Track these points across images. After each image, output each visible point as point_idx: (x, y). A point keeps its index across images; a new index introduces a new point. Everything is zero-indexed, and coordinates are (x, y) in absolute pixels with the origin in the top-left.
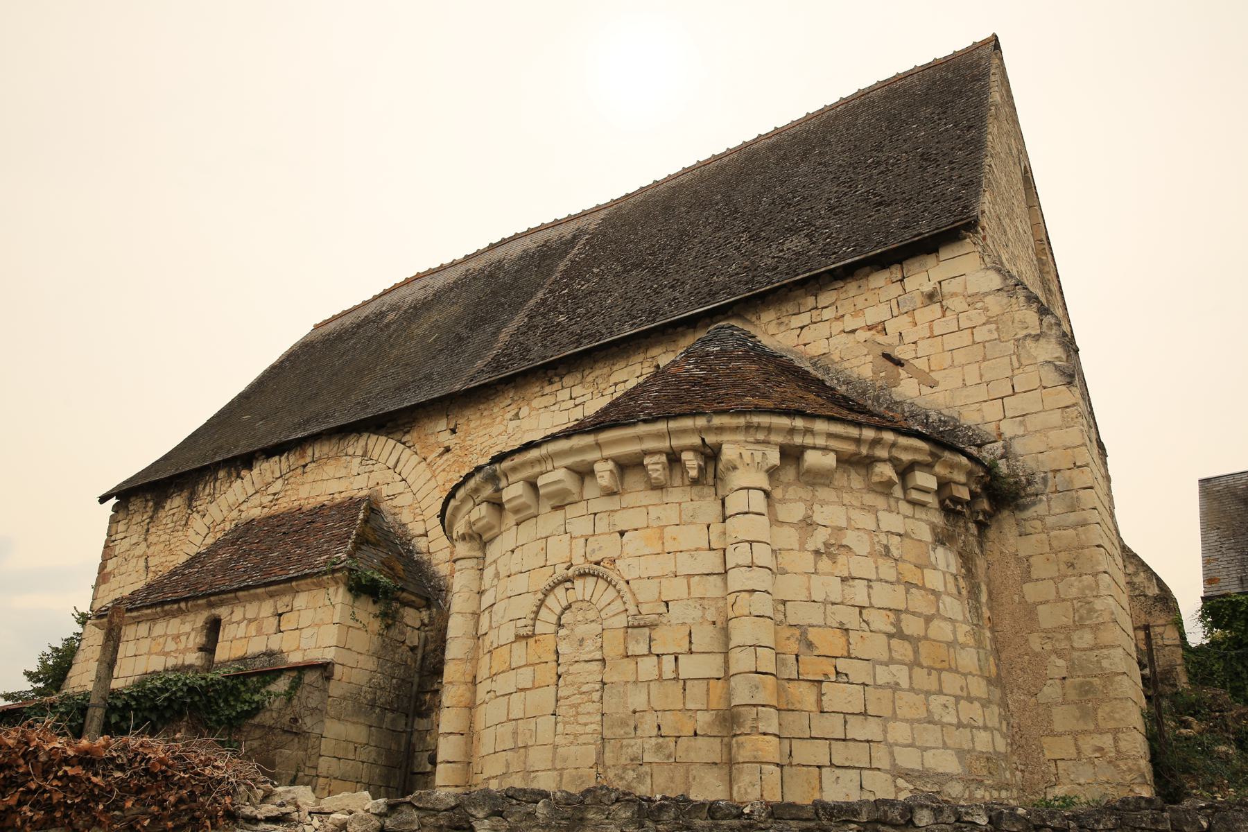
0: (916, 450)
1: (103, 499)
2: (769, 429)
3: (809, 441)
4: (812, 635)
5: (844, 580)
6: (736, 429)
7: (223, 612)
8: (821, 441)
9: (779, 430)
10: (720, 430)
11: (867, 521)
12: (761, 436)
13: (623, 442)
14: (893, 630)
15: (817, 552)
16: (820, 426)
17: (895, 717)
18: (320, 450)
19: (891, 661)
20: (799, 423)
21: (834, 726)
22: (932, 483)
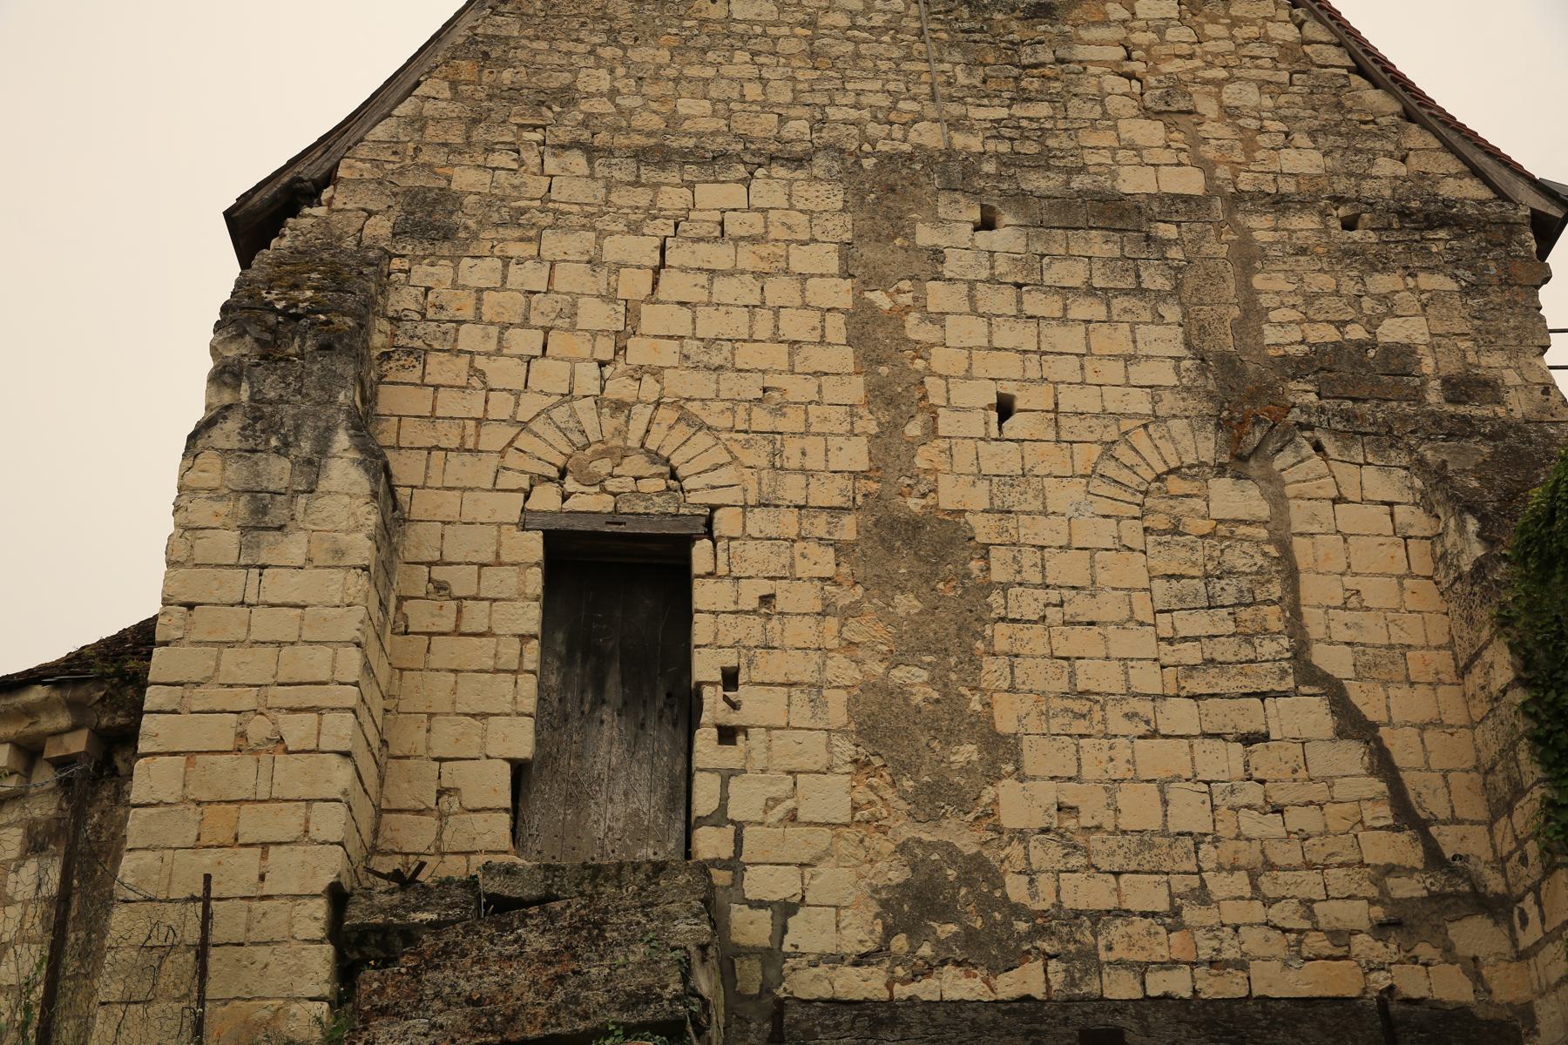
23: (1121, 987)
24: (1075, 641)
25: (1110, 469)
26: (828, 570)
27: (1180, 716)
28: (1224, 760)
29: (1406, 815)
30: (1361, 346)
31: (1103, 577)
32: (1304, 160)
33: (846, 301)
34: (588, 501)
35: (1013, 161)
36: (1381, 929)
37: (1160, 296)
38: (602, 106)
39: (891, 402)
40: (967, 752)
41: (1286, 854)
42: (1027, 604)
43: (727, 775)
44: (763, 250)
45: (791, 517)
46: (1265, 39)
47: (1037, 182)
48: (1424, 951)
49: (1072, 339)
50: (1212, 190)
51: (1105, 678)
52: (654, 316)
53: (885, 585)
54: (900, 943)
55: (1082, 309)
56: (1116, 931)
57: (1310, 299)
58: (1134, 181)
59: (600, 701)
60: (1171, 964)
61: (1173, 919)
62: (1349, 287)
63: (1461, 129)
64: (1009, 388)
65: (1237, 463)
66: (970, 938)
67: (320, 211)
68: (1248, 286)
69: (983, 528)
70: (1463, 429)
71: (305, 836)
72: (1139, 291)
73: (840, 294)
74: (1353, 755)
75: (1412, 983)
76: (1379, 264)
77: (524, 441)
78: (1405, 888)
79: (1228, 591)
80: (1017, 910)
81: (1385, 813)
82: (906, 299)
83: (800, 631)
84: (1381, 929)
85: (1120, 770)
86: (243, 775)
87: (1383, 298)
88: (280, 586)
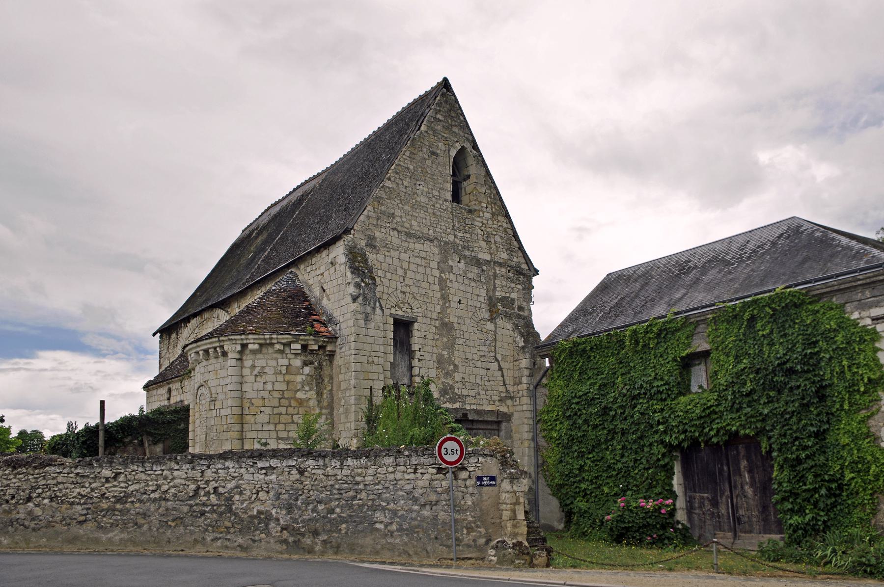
0: (287, 338)
1: (154, 335)
2: (236, 340)
3: (248, 341)
4: (253, 401)
5: (264, 383)
6: (227, 340)
7: (171, 386)
8: (252, 341)
9: (238, 340)
10: (223, 341)
11: (274, 363)
12: (234, 342)
13: (204, 345)
14: (281, 397)
15: (256, 375)
16: (250, 337)
17: (279, 423)
18: (206, 315)
19: (280, 406)
20: (243, 337)
21: (259, 427)
22: (299, 347)
23: (468, 407)
24: (467, 349)
25: (474, 317)
26: (434, 332)
27: (479, 364)
28: (484, 372)
29: (504, 384)
30: (509, 297)
31: (375, 220)
32: (504, 255)
33: (438, 275)
34: (400, 313)
35: (463, 247)
36: (499, 401)
37: (484, 283)
38: (399, 220)
39: (444, 299)
40: (451, 367)
41: (489, 388)
42: (461, 341)
43: (420, 368)
44: (426, 261)
45: (429, 320)
46: (502, 226)
47: (467, 253)
48: (504, 404)
49: (470, 289)
50: (492, 260)
51: (469, 356)
52: (410, 274)
53: (441, 335)
54: (442, 398)
55: (473, 284)
56: (468, 398)
57: (503, 286)
58: (481, 256)
59: (397, 349)
60: (474, 404)
61: (475, 397)
62: (508, 285)
63: (530, 260)
64: (461, 298)
65: (492, 319)
66: (450, 398)
67: (351, 236)
68: (494, 282)
69: (456, 327)
70: (519, 317)
71: (378, 379)
72: (480, 281)
73: (436, 273)
74: (500, 373)
75: (501, 409)
76: (512, 281)
77: (390, 298)
78: (503, 395)
79: (488, 343)
80: (456, 394)
81: (502, 383)
82: (447, 277)
83: (430, 342)
84: (499, 401)
85: (471, 373)
86: (368, 367)
87: (512, 288)
88: (371, 332)
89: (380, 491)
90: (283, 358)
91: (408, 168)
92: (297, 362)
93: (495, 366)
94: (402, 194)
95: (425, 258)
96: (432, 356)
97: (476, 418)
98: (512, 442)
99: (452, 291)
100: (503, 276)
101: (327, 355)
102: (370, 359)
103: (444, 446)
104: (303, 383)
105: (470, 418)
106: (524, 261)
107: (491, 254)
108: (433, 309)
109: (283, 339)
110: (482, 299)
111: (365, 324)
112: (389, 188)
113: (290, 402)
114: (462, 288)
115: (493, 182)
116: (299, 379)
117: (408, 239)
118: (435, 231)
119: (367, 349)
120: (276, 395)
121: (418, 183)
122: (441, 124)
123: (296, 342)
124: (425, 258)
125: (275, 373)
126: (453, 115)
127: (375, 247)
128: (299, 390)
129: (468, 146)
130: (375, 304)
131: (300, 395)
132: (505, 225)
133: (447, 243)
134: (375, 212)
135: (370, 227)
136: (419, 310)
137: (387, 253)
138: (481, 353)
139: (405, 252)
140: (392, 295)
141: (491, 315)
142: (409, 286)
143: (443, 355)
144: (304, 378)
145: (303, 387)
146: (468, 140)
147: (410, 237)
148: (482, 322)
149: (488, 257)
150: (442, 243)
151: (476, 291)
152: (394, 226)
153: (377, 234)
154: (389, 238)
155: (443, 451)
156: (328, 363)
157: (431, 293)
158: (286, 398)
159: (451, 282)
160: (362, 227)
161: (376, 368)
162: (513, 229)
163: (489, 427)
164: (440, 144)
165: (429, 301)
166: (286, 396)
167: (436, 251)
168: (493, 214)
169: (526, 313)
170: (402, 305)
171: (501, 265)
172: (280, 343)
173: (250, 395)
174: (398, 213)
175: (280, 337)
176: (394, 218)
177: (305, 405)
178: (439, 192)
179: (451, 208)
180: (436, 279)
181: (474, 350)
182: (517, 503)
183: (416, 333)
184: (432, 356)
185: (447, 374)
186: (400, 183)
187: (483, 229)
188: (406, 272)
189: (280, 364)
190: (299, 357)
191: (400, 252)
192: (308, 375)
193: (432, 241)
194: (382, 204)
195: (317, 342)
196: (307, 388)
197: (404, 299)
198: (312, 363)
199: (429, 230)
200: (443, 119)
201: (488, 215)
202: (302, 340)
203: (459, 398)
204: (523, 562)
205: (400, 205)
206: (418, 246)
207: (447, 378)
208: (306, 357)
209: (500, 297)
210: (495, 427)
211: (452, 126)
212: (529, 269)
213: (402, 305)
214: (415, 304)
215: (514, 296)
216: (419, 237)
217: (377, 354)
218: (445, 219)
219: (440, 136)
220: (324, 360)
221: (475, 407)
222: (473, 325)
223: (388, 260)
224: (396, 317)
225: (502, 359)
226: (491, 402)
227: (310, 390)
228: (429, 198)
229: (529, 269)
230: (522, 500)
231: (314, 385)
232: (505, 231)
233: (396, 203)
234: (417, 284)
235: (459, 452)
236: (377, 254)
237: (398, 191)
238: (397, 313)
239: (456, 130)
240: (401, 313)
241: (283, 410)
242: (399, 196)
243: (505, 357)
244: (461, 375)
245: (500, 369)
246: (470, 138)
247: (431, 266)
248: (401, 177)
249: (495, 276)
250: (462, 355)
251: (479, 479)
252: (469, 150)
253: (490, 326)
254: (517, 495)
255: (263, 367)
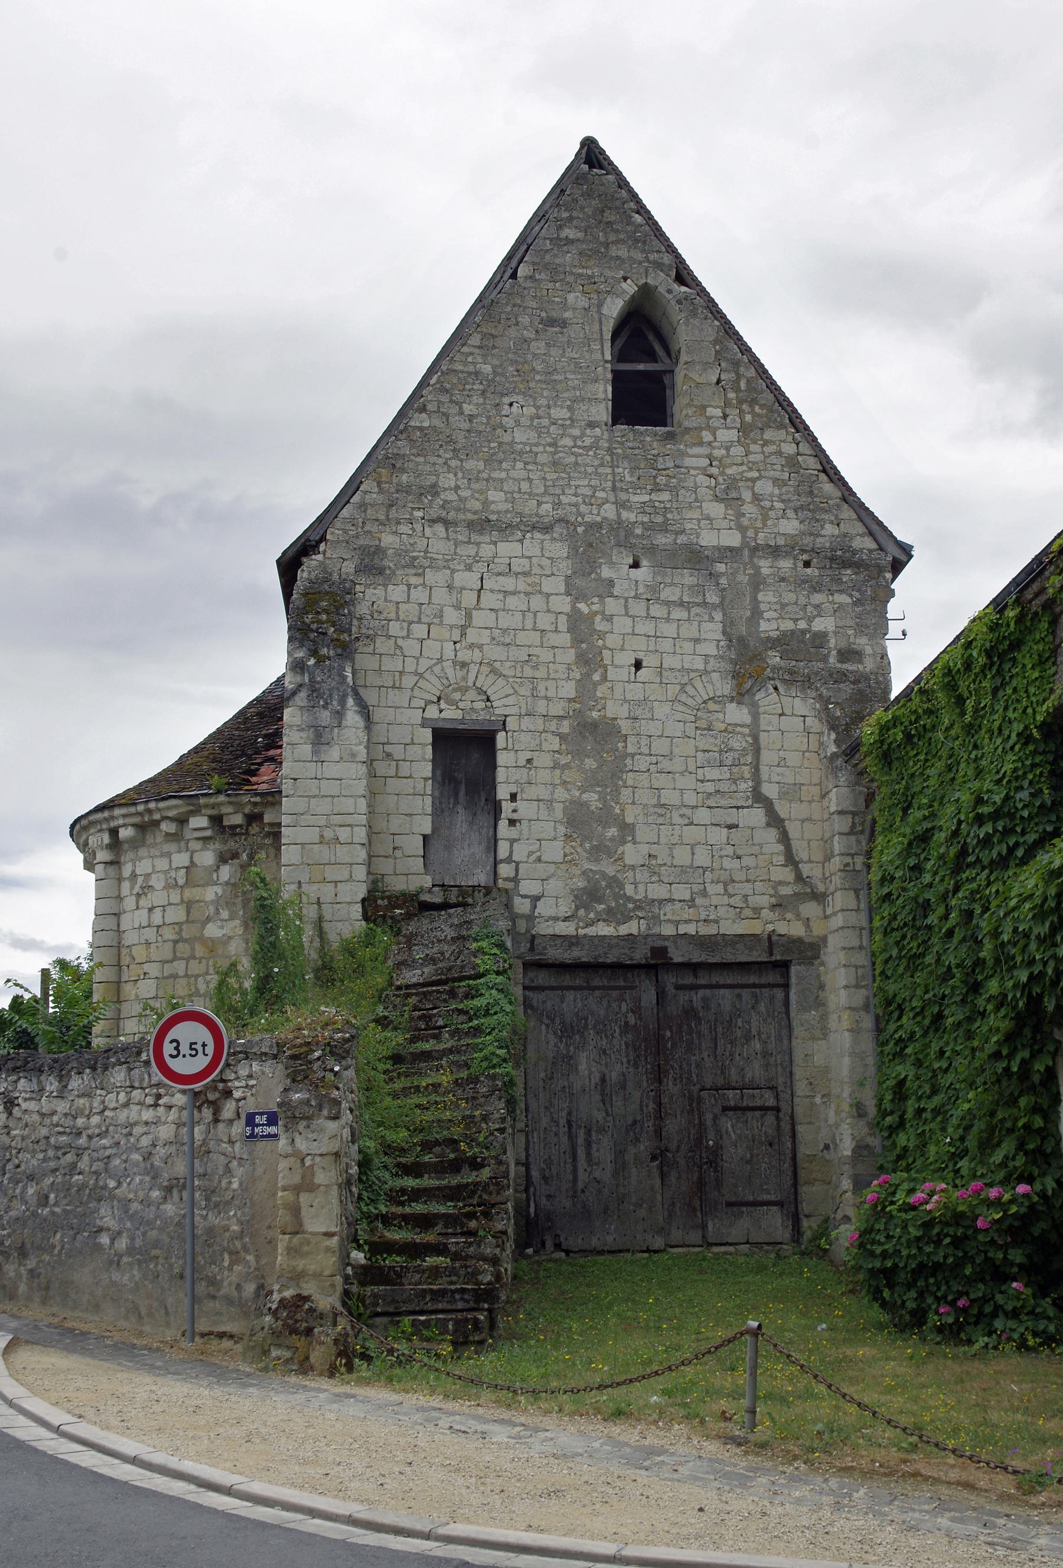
0: (176, 807)
8: (121, 822)
11: (162, 864)
14: (177, 937)
19: (175, 958)
23: (668, 930)
24: (662, 781)
25: (683, 698)
26: (556, 747)
27: (703, 815)
28: (719, 835)
29: (791, 859)
30: (803, 632)
32: (790, 526)
33: (567, 608)
34: (451, 713)
36: (773, 907)
37: (714, 607)
39: (587, 663)
40: (612, 832)
42: (642, 763)
43: (512, 842)
44: (530, 580)
46: (779, 453)
49: (669, 629)
50: (745, 544)
51: (670, 797)
53: (579, 754)
55: (678, 614)
56: (668, 908)
58: (708, 539)
61: (691, 903)
63: (880, 524)
65: (740, 696)
66: (610, 911)
67: (320, 557)
70: (841, 677)
72: (704, 604)
74: (772, 834)
75: (782, 928)
76: (816, 588)
78: (785, 891)
80: (629, 899)
81: (781, 860)
82: (595, 608)
83: (544, 775)
84: (773, 907)
86: (324, 853)
87: (817, 607)
89: (108, 1152)
90: (180, 852)
91: (477, 373)
92: (207, 858)
93: (756, 816)
94: (460, 437)
95: (526, 574)
96: (550, 808)
97: (697, 957)
98: (824, 1018)
99: (611, 640)
100: (783, 580)
101: (268, 835)
102: (328, 834)
103: (170, 1036)
104: (217, 902)
105: (677, 959)
106: (860, 528)
107: (743, 530)
108: (551, 693)
109: (169, 808)
110: (711, 649)
111: (315, 752)
112: (421, 429)
113: (193, 949)
114: (647, 628)
115: (746, 350)
116: (211, 893)
117: (475, 537)
118: (557, 505)
119: (319, 811)
120: (169, 934)
121: (506, 400)
122: (574, 250)
123: (196, 812)
124: (526, 574)
125: (167, 887)
126: (613, 218)
127: (381, 571)
128: (208, 919)
129: (662, 282)
130: (343, 702)
131: (212, 931)
132: (789, 449)
133: (594, 527)
134: (381, 491)
135: (367, 528)
136: (511, 700)
137: (414, 580)
138: (710, 787)
139: (469, 568)
140: (427, 675)
141: (740, 685)
142: (480, 647)
143: (585, 805)
144: (220, 891)
145: (217, 912)
146: (659, 266)
147: (481, 532)
148: (712, 706)
149: (733, 539)
150: (580, 530)
151: (690, 631)
152: (434, 513)
153: (388, 540)
154: (421, 544)
155: (168, 1049)
156: (272, 851)
157: (545, 655)
158: (186, 941)
159: (609, 619)
160: (345, 531)
161: (342, 853)
162: (820, 453)
163: (753, 979)
164: (571, 297)
165: (541, 673)
166: (185, 936)
167: (560, 550)
168: (744, 429)
169: (869, 665)
170: (457, 696)
171: (775, 552)
172: (167, 818)
173: (130, 938)
174: (447, 480)
175: (162, 805)
176: (436, 494)
177: (220, 952)
178: (569, 408)
179: (609, 441)
180: (563, 619)
181: (683, 782)
182: (306, 1185)
183: (502, 758)
184: (550, 808)
185: (599, 851)
186: (454, 410)
187: (714, 471)
188: (469, 616)
189: (174, 866)
190: (212, 847)
191: (453, 571)
192: (227, 883)
193: (547, 529)
194: (403, 470)
195: (238, 807)
196: (225, 914)
197: (465, 679)
198: (235, 855)
199: (539, 504)
200: (580, 235)
201: (728, 435)
202: (206, 806)
203: (638, 908)
204: (288, 1354)
205: (453, 463)
206: (507, 549)
207: (597, 860)
208: (225, 842)
209: (774, 634)
210: (772, 977)
211: (607, 245)
212: (881, 549)
213: (457, 696)
214: (497, 689)
215: (824, 624)
216: (510, 526)
217: (349, 820)
218: (590, 470)
219: (570, 279)
220: (261, 847)
221: (691, 929)
222: (679, 716)
223: (419, 595)
224: (440, 725)
225: (782, 795)
226: (748, 912)
227: (231, 918)
228: (539, 431)
229: (881, 549)
230: (320, 1178)
231: (239, 906)
232: (792, 463)
233: (440, 461)
234: (504, 638)
235: (210, 1050)
236: (385, 586)
237: (448, 432)
238: (444, 715)
239: (622, 252)
240: (457, 715)
241: (180, 967)
242: (451, 441)
243: (790, 792)
244: (645, 849)
245: (775, 820)
246: (667, 259)
247: (545, 589)
248: (458, 397)
249: (757, 583)
250: (645, 797)
251: (250, 1120)
252: (662, 290)
253: (737, 714)
254: (308, 1162)
255: (148, 876)
